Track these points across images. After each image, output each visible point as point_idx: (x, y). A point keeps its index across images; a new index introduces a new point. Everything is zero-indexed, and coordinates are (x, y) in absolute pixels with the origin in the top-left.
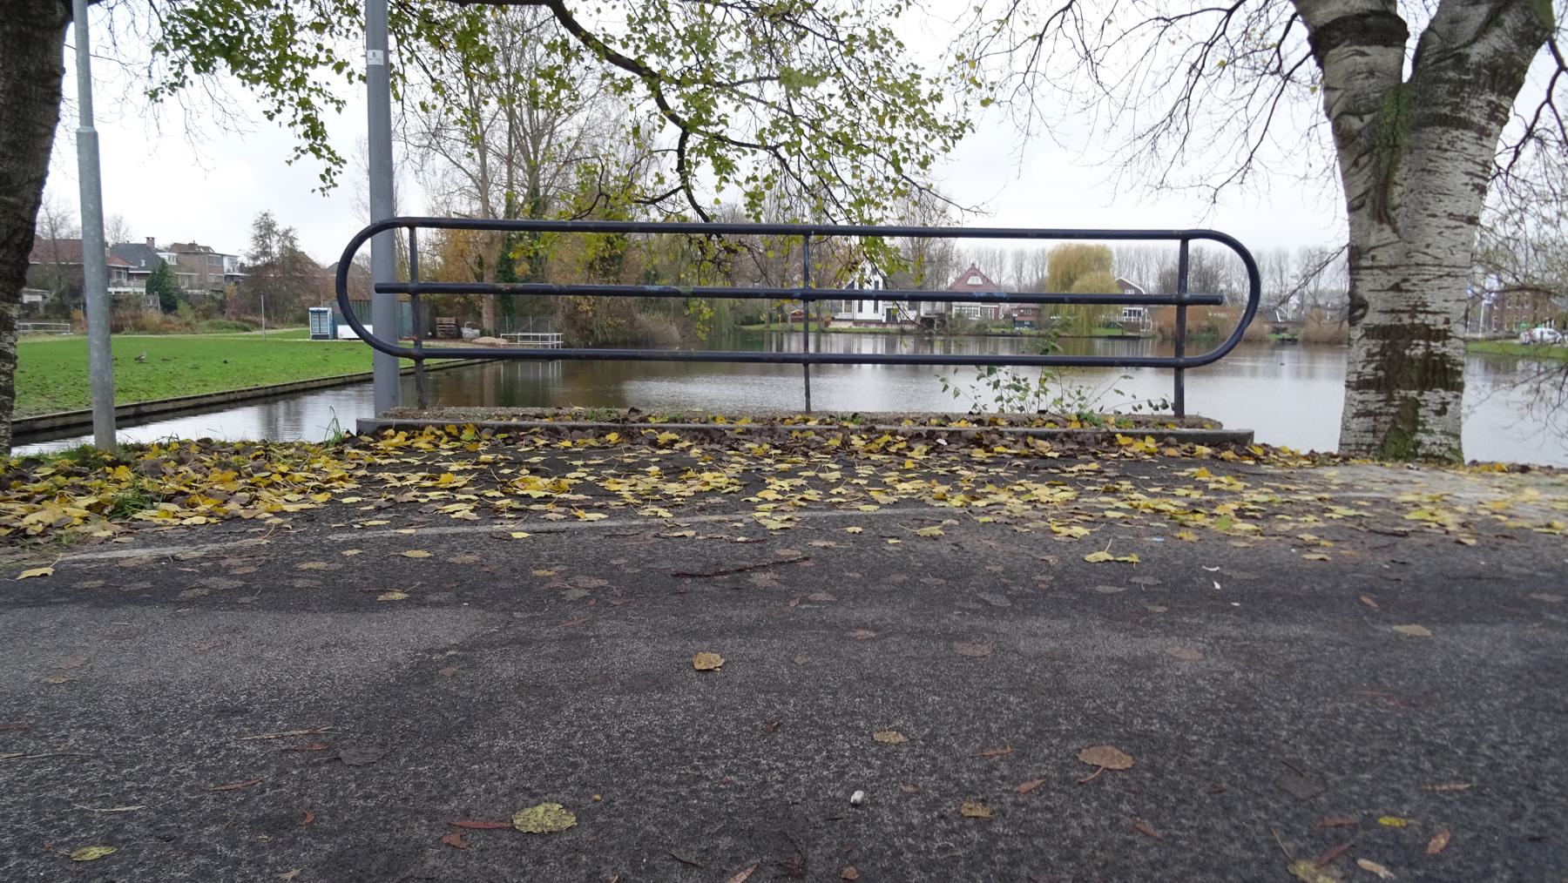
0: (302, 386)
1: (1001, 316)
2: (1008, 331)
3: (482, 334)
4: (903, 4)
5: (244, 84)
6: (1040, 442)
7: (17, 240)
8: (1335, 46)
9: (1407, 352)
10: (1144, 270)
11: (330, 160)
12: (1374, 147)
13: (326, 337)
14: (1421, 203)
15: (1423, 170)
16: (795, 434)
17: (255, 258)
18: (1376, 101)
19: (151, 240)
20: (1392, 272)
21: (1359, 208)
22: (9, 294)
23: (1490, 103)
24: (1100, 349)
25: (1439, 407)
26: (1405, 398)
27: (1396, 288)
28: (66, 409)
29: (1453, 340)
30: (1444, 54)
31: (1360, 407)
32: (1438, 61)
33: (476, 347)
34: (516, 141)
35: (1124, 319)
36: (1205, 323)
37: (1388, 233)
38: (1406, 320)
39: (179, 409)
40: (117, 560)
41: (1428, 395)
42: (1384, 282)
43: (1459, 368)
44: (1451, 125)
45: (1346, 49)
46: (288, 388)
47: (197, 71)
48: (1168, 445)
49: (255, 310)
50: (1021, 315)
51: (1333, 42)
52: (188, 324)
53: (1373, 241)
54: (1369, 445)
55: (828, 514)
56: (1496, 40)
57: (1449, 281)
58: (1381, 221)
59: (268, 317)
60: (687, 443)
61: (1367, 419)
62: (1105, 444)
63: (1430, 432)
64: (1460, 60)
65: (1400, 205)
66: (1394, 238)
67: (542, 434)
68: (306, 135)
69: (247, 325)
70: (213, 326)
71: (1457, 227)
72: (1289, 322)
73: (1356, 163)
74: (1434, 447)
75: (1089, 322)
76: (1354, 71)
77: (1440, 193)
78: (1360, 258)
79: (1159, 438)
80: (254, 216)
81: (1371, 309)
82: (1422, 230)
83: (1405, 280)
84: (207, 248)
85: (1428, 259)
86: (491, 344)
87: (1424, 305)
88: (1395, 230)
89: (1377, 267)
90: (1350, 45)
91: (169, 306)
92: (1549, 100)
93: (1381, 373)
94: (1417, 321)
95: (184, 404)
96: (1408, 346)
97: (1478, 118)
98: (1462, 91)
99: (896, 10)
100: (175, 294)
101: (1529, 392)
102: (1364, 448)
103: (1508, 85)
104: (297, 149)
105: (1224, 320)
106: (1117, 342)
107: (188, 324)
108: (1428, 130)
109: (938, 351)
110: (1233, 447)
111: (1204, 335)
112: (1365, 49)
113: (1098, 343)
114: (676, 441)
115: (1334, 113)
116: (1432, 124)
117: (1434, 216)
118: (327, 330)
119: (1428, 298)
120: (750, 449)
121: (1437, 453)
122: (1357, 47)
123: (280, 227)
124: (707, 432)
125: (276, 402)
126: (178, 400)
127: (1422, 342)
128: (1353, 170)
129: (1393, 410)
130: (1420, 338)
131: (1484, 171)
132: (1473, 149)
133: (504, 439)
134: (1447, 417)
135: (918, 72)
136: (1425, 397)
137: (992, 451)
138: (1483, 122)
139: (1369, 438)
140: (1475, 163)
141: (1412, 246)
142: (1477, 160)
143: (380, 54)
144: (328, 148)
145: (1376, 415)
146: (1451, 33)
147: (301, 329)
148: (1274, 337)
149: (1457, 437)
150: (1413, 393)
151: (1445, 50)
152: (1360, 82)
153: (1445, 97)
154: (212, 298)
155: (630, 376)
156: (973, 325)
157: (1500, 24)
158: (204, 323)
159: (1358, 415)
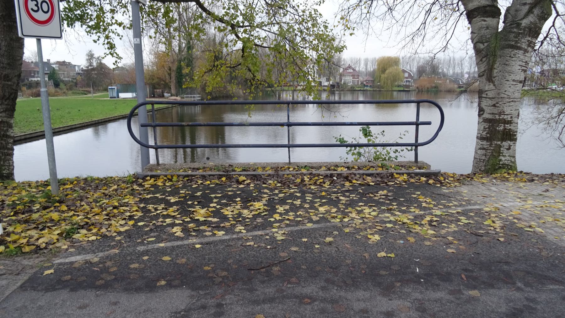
0: (108, 119)
1: (360, 83)
2: (362, 89)
3: (172, 96)
4: (322, 1)
5: (88, 34)
6: (368, 178)
7: (12, 97)
8: (475, 17)
9: (497, 128)
10: (412, 65)
11: (117, 57)
12: (488, 55)
13: (115, 98)
14: (503, 76)
15: (505, 64)
16: (285, 176)
17: (87, 67)
18: (489, 38)
19: (49, 60)
20: (493, 100)
21: (482, 76)
22: (10, 115)
23: (528, 41)
24: (396, 96)
25: (508, 147)
26: (496, 144)
27: (494, 105)
28: (25, 132)
29: (513, 124)
30: (513, 22)
31: (481, 146)
32: (511, 25)
33: (169, 100)
34: (181, 23)
35: (404, 84)
36: (434, 85)
37: (492, 86)
38: (497, 117)
39: (65, 130)
40: (72, 263)
41: (504, 143)
42: (490, 103)
43: (515, 133)
44: (515, 49)
45: (479, 19)
46: (103, 121)
47: (68, 26)
48: (412, 177)
49: (88, 86)
50: (367, 83)
51: (474, 16)
52: (64, 93)
53: (487, 88)
54: (484, 160)
55: (297, 228)
56: (531, 19)
57: (512, 104)
58: (490, 82)
59: (94, 89)
60: (249, 181)
61: (483, 151)
62: (390, 177)
63: (505, 156)
64: (519, 25)
65: (496, 76)
66: (494, 88)
67: (200, 178)
68: (108, 48)
69: (86, 92)
70: (73, 93)
71: (516, 85)
72: (464, 84)
73: (481, 60)
74: (506, 161)
75: (392, 85)
76: (482, 27)
77: (510, 73)
78: (482, 94)
79: (409, 174)
80: (86, 52)
81: (485, 112)
82: (503, 86)
83: (497, 103)
84: (69, 63)
85: (505, 96)
86: (175, 99)
87: (504, 112)
88: (494, 85)
89: (488, 98)
90: (480, 18)
91: (57, 85)
92: (553, 25)
93: (488, 135)
94: (501, 118)
95: (66, 128)
96: (498, 126)
97: (524, 46)
98: (519, 36)
99: (319, 3)
100: (59, 80)
101: (545, 124)
102: (482, 161)
103: (535, 34)
104: (105, 54)
105: (440, 84)
106: (402, 93)
107: (64, 93)
108: (506, 50)
109: (337, 99)
110: (433, 178)
111: (433, 89)
112: (486, 19)
113: (395, 93)
114: (245, 180)
115: (475, 42)
116: (508, 48)
117: (508, 81)
118: (115, 95)
119: (505, 109)
120: (270, 183)
121: (507, 163)
122: (482, 18)
123: (96, 56)
124: (255, 176)
125: (99, 125)
126: (64, 127)
127: (502, 125)
128: (480, 62)
129: (492, 148)
130: (502, 123)
131: (526, 65)
132: (522, 57)
133: (187, 180)
134: (510, 151)
135: (327, 25)
136: (503, 144)
137: (352, 183)
138: (526, 48)
139: (484, 158)
140: (523, 62)
141: (500, 91)
142: (524, 61)
143: (138, 39)
144: (116, 53)
145: (486, 150)
146: (516, 15)
147: (105, 93)
148: (459, 90)
149: (514, 157)
150: (499, 143)
151: (513, 21)
152: (483, 31)
153: (513, 38)
154: (72, 81)
155: (225, 112)
156: (349, 87)
157: (533, 13)
158: (70, 92)
159: (480, 149)
